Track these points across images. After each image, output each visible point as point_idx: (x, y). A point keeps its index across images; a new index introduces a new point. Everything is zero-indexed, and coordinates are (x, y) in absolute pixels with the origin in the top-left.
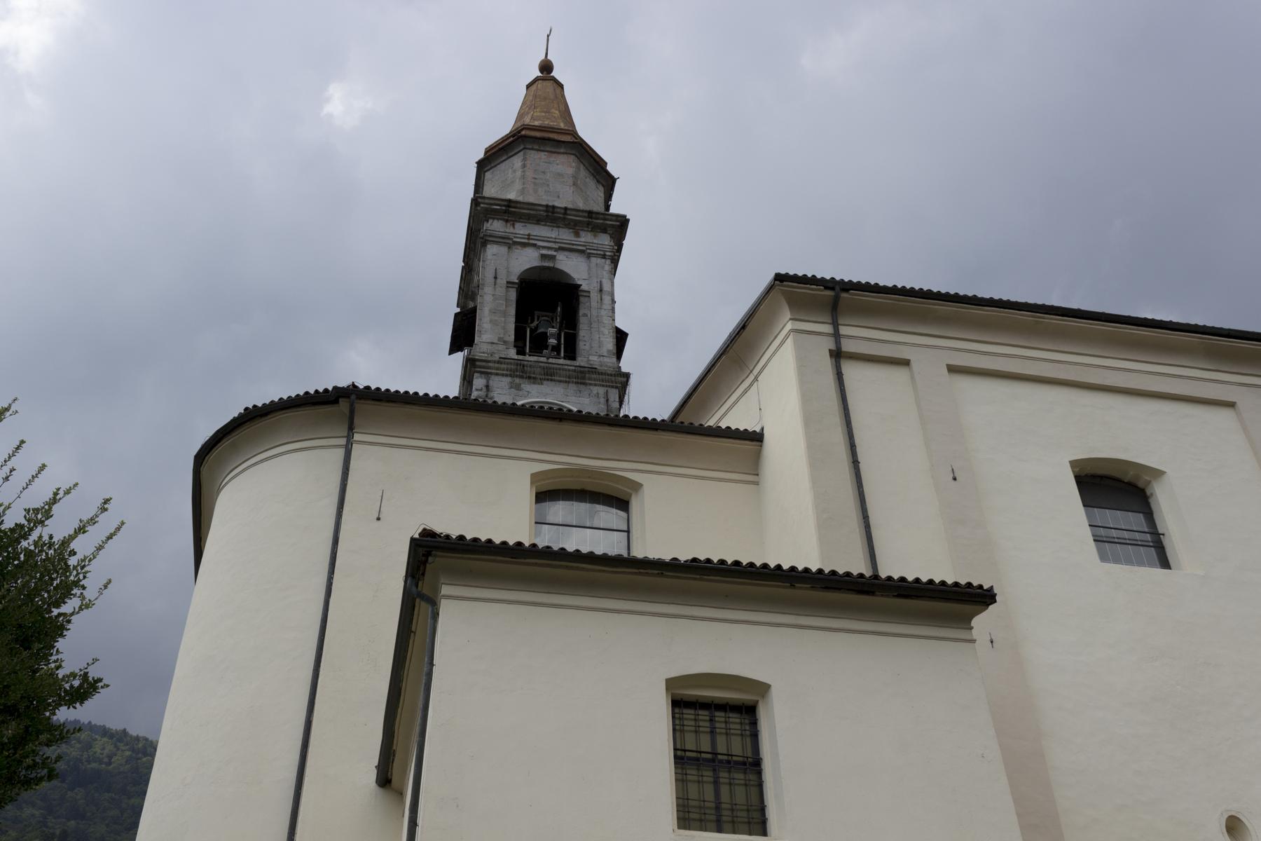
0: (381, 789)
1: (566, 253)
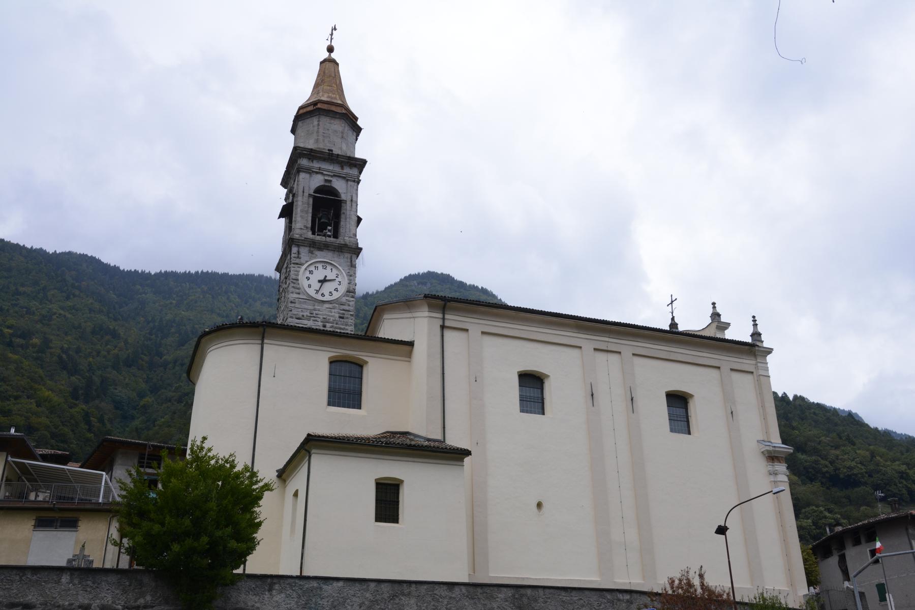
0: (278, 479)
1: (337, 178)
